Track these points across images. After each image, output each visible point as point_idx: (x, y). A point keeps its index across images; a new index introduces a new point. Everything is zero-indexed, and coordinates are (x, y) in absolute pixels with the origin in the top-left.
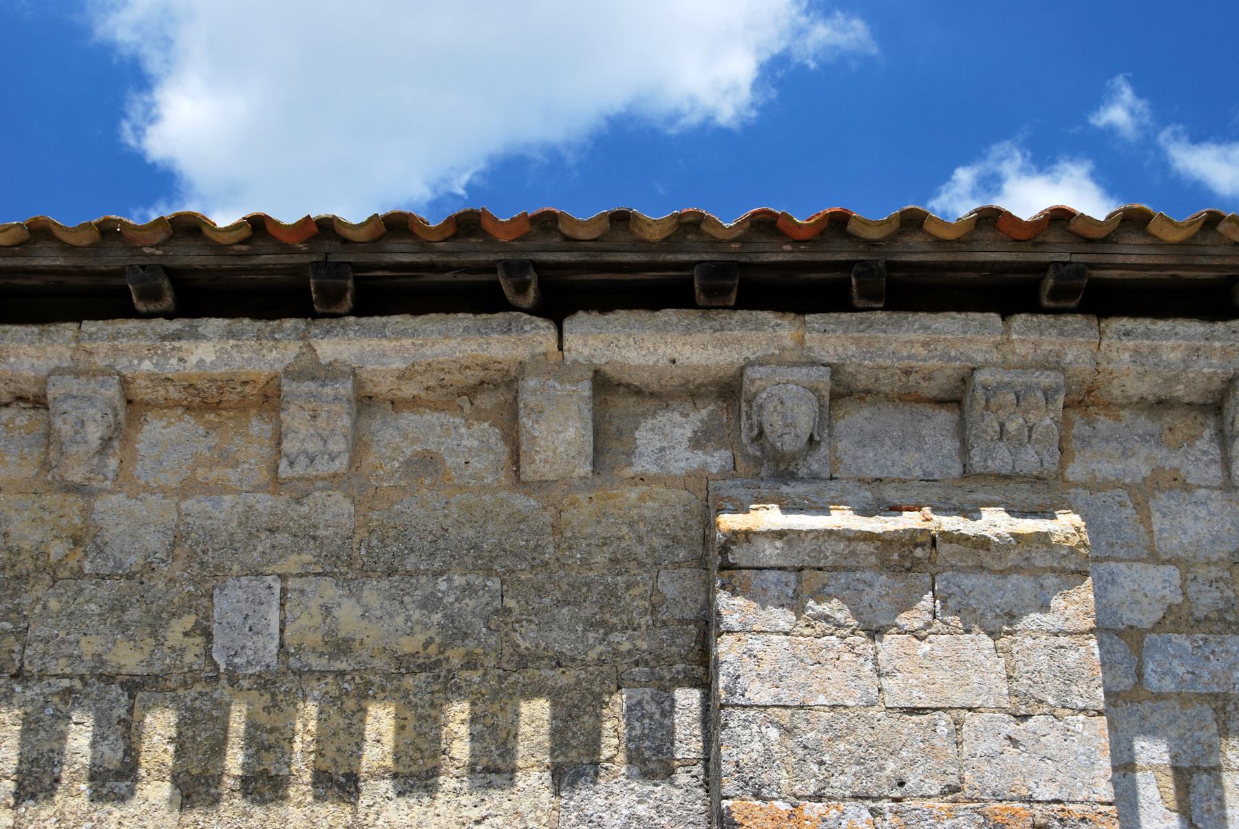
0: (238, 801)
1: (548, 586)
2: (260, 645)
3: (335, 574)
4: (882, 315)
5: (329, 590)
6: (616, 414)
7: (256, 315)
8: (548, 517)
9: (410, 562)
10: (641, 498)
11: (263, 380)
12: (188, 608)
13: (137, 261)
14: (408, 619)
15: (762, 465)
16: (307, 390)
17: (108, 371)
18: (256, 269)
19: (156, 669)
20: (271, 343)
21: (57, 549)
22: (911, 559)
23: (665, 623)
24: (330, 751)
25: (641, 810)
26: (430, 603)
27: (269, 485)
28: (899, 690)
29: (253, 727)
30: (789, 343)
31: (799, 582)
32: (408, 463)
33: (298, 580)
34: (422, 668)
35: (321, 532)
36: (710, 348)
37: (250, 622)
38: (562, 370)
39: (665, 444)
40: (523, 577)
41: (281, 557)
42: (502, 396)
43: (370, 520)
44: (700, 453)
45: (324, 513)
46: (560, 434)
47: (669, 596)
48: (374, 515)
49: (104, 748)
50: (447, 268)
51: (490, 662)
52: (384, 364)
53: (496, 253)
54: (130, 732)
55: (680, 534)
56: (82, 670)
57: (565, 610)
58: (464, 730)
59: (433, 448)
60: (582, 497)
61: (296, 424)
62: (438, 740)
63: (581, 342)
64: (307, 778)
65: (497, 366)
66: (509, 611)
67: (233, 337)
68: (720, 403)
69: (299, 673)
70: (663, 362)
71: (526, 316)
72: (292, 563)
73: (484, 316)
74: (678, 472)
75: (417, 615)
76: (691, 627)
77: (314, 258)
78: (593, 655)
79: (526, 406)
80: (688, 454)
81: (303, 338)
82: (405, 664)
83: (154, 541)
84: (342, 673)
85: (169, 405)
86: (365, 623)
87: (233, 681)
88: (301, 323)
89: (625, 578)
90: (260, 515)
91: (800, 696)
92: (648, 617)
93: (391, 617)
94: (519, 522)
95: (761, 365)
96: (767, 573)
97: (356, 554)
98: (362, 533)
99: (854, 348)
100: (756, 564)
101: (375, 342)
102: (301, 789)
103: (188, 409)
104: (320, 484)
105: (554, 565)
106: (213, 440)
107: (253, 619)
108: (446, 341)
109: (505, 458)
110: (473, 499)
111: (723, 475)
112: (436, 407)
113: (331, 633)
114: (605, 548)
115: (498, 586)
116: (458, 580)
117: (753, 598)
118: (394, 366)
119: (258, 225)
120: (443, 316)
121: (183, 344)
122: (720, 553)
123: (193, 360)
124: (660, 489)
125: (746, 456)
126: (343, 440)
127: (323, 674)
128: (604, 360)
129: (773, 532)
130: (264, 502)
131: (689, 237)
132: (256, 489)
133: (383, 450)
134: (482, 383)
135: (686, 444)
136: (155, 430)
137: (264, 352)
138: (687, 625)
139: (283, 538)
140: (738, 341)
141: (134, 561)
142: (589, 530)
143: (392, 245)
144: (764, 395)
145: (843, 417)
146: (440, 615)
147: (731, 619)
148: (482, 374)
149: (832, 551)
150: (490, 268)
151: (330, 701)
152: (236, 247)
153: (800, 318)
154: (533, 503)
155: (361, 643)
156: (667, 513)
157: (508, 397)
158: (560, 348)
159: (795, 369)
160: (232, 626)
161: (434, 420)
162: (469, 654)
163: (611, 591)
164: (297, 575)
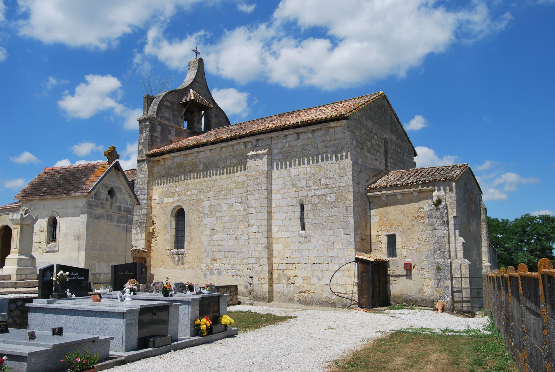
22: (257, 155)
28: (257, 164)
107: (229, 162)
136: (223, 149)
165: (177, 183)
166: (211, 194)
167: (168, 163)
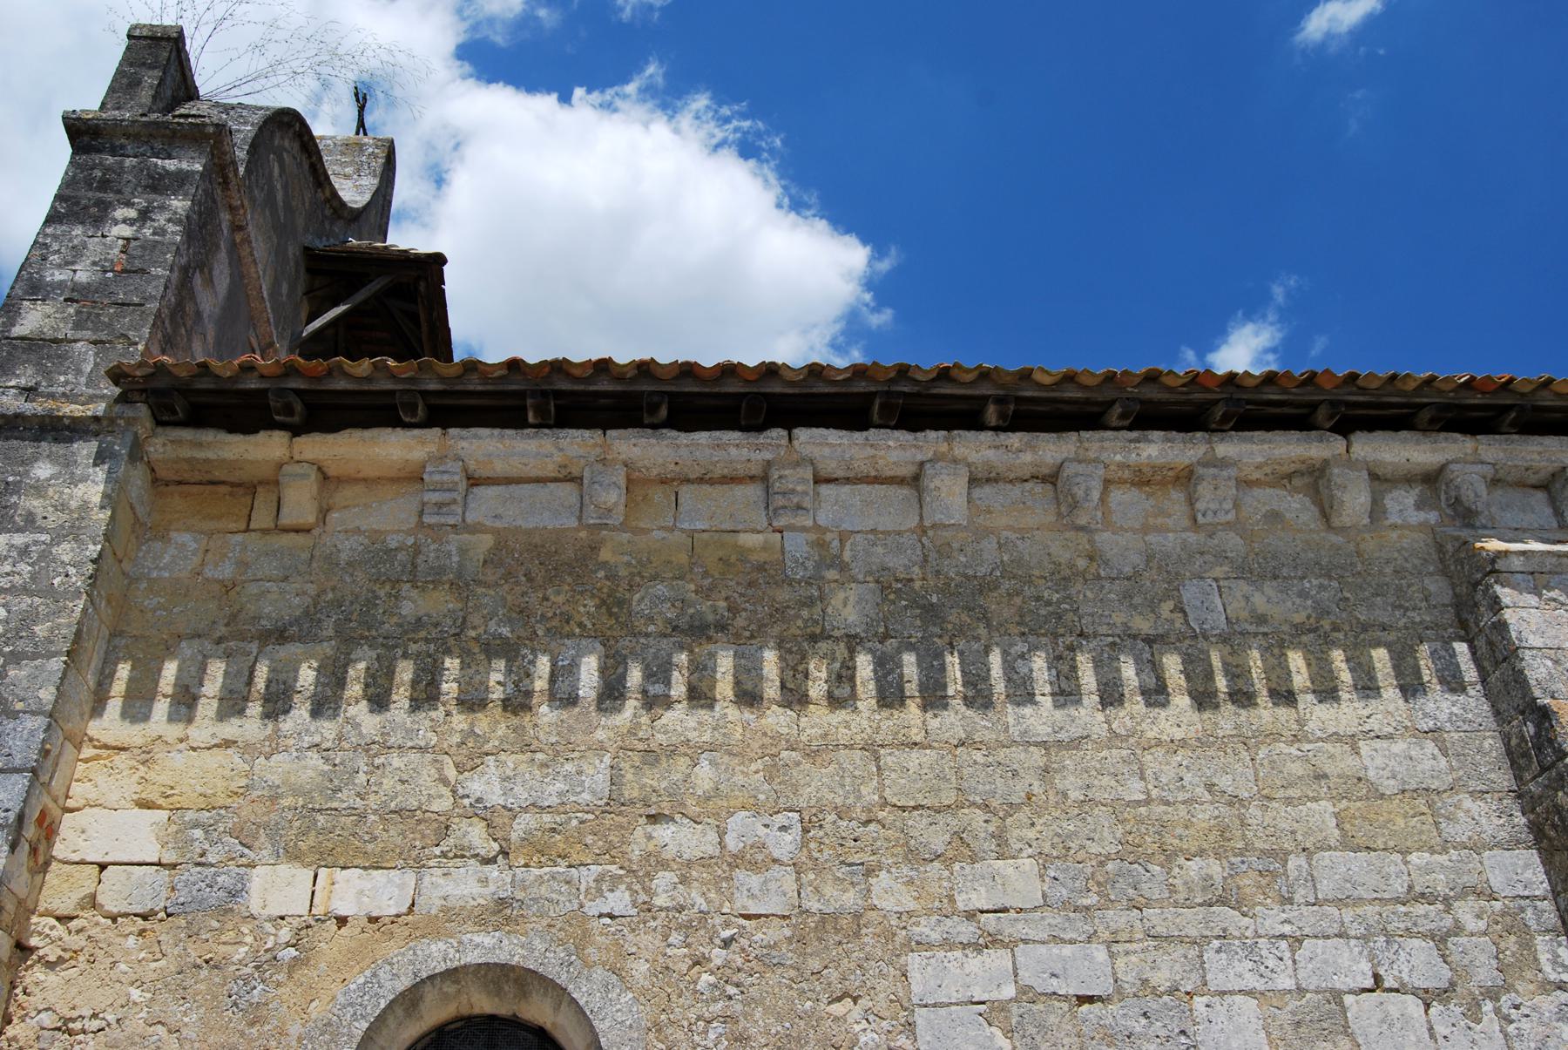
0: (1230, 706)
4: (1516, 437)
5: (1243, 587)
7: (1179, 431)
8: (1352, 546)
9: (1285, 571)
12: (1166, 596)
13: (1125, 395)
17: (1097, 460)
19: (1161, 631)
21: (1081, 563)
24: (1274, 677)
25: (1454, 709)
26: (1303, 594)
29: (1225, 664)
32: (1264, 516)
34: (1310, 631)
38: (1351, 464)
42: (1307, 480)
49: (1143, 676)
51: (1347, 628)
54: (1156, 668)
56: (1118, 632)
58: (1344, 666)
60: (1367, 536)
62: (1331, 671)
64: (1265, 693)
69: (1241, 633)
72: (1218, 572)
75: (1298, 601)
78: (1401, 624)
82: (1299, 630)
83: (1137, 559)
84: (1265, 634)
85: (1122, 482)
87: (1206, 638)
91: (1555, 644)
98: (1252, 556)
102: (1263, 698)
103: (1133, 484)
106: (1152, 502)
107: (1212, 603)
113: (1253, 611)
116: (1315, 582)
119: (514, 365)
121: (1141, 445)
123: (1145, 454)
127: (1256, 635)
130: (1192, 537)
139: (1208, 557)
141: (1128, 570)
143: (1266, 389)
147: (1506, 600)
149: (1550, 562)
151: (1265, 650)
162: (1333, 623)
163: (1399, 589)
165: (492, 725)
166: (1019, 879)
167: (391, 518)
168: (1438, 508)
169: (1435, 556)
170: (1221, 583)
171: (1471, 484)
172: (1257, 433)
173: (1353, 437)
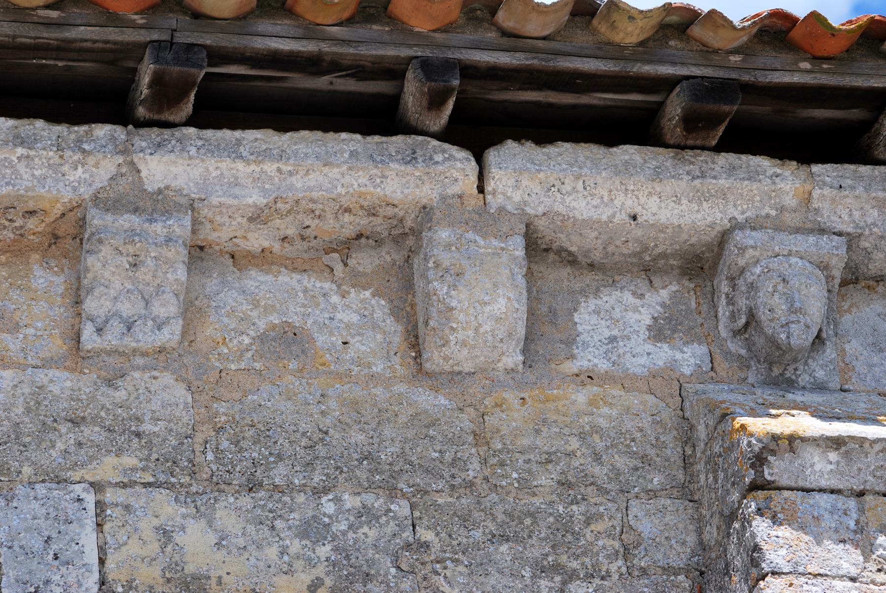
1: (476, 514)
2: (71, 579)
3: (173, 485)
5: (166, 507)
6: (545, 289)
7: (53, 118)
8: (466, 421)
9: (279, 474)
10: (592, 402)
11: (58, 209)
14: (283, 552)
15: (748, 367)
16: (127, 225)
18: (63, 49)
20: (78, 156)
23: (644, 572)
26: (313, 530)
27: (65, 358)
30: (790, 201)
31: (862, 511)
32: (262, 338)
33: (121, 491)
35: (147, 427)
36: (684, 201)
37: (54, 547)
38: (486, 220)
39: (615, 332)
40: (440, 501)
41: (92, 459)
42: (388, 255)
43: (216, 414)
44: (665, 347)
45: (149, 401)
46: (482, 307)
47: (645, 535)
48: (221, 408)
50: (334, 66)
52: (236, 197)
53: (410, 46)
55: (652, 452)
57: (504, 548)
59: (296, 321)
60: (511, 397)
61: (107, 274)
63: (511, 182)
65: (390, 211)
66: (425, 546)
67: (22, 144)
68: (686, 283)
70: (622, 217)
71: (435, 143)
72: (108, 468)
73: (377, 138)
74: (639, 371)
75: (295, 546)
76: (681, 578)
77: (155, 36)
79: (437, 265)
80: (649, 347)
81: (124, 152)
86: (220, 555)
88: (120, 132)
89: (583, 508)
90: (56, 399)
92: (620, 562)
93: (259, 547)
94: (428, 427)
95: (754, 229)
96: (817, 496)
97: (200, 459)
98: (205, 431)
99: (876, 213)
100: (801, 483)
101: (226, 164)
104: (139, 361)
105: (482, 487)
108: (326, 170)
109: (397, 339)
110: (358, 392)
111: (699, 376)
112: (294, 266)
113: (175, 566)
114: (550, 466)
115: (407, 511)
116: (350, 501)
117: (802, 528)
118: (250, 201)
120: (319, 134)
122: (753, 466)
124: (617, 392)
125: (727, 354)
126: (174, 300)
128: (541, 210)
129: (829, 439)
130: (61, 383)
131: (672, 43)
132: (46, 364)
133: (226, 320)
134: (359, 236)
135: (644, 334)
137: (66, 168)
138: (676, 574)
139: (92, 433)
140: (723, 194)
142: (525, 442)
143: (264, 25)
144: (758, 270)
145: (849, 311)
146: (328, 547)
147: (775, 556)
148: (364, 221)
150: (394, 72)
152: (41, 12)
153: (804, 167)
154: (443, 401)
155: (220, 581)
156: (629, 424)
157: (397, 258)
158: (481, 190)
159: (799, 237)
160: (28, 553)
161: (294, 283)
164: (117, 484)
168: (709, 338)
169: (673, 452)
170: (109, 496)
171: (791, 288)
172: (251, 135)
173: (492, 156)
